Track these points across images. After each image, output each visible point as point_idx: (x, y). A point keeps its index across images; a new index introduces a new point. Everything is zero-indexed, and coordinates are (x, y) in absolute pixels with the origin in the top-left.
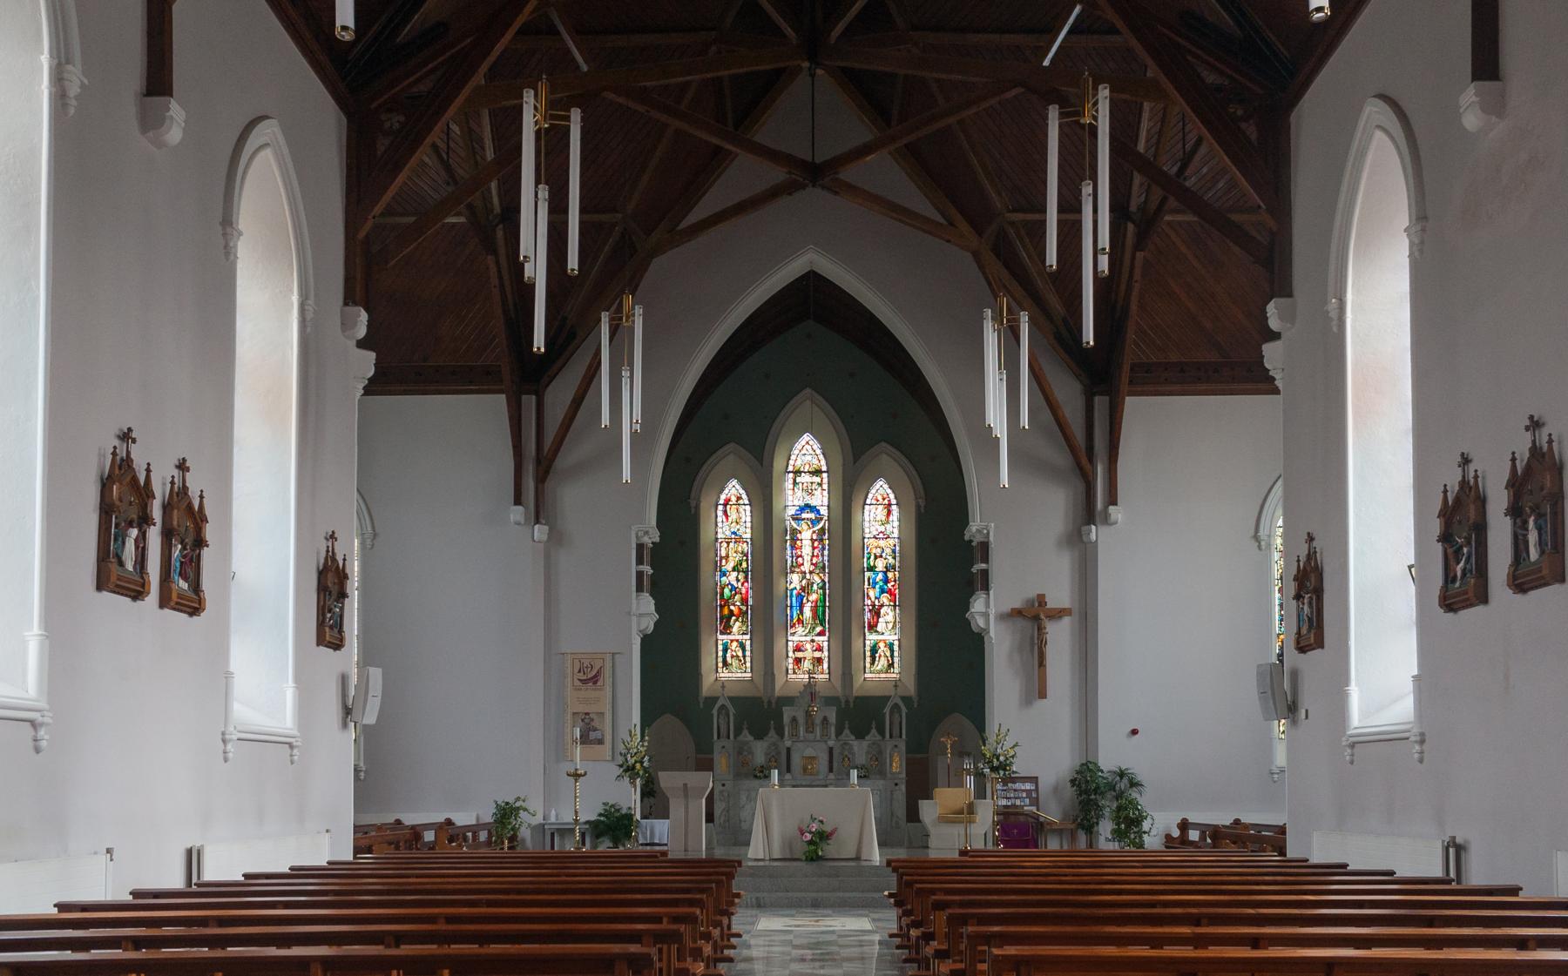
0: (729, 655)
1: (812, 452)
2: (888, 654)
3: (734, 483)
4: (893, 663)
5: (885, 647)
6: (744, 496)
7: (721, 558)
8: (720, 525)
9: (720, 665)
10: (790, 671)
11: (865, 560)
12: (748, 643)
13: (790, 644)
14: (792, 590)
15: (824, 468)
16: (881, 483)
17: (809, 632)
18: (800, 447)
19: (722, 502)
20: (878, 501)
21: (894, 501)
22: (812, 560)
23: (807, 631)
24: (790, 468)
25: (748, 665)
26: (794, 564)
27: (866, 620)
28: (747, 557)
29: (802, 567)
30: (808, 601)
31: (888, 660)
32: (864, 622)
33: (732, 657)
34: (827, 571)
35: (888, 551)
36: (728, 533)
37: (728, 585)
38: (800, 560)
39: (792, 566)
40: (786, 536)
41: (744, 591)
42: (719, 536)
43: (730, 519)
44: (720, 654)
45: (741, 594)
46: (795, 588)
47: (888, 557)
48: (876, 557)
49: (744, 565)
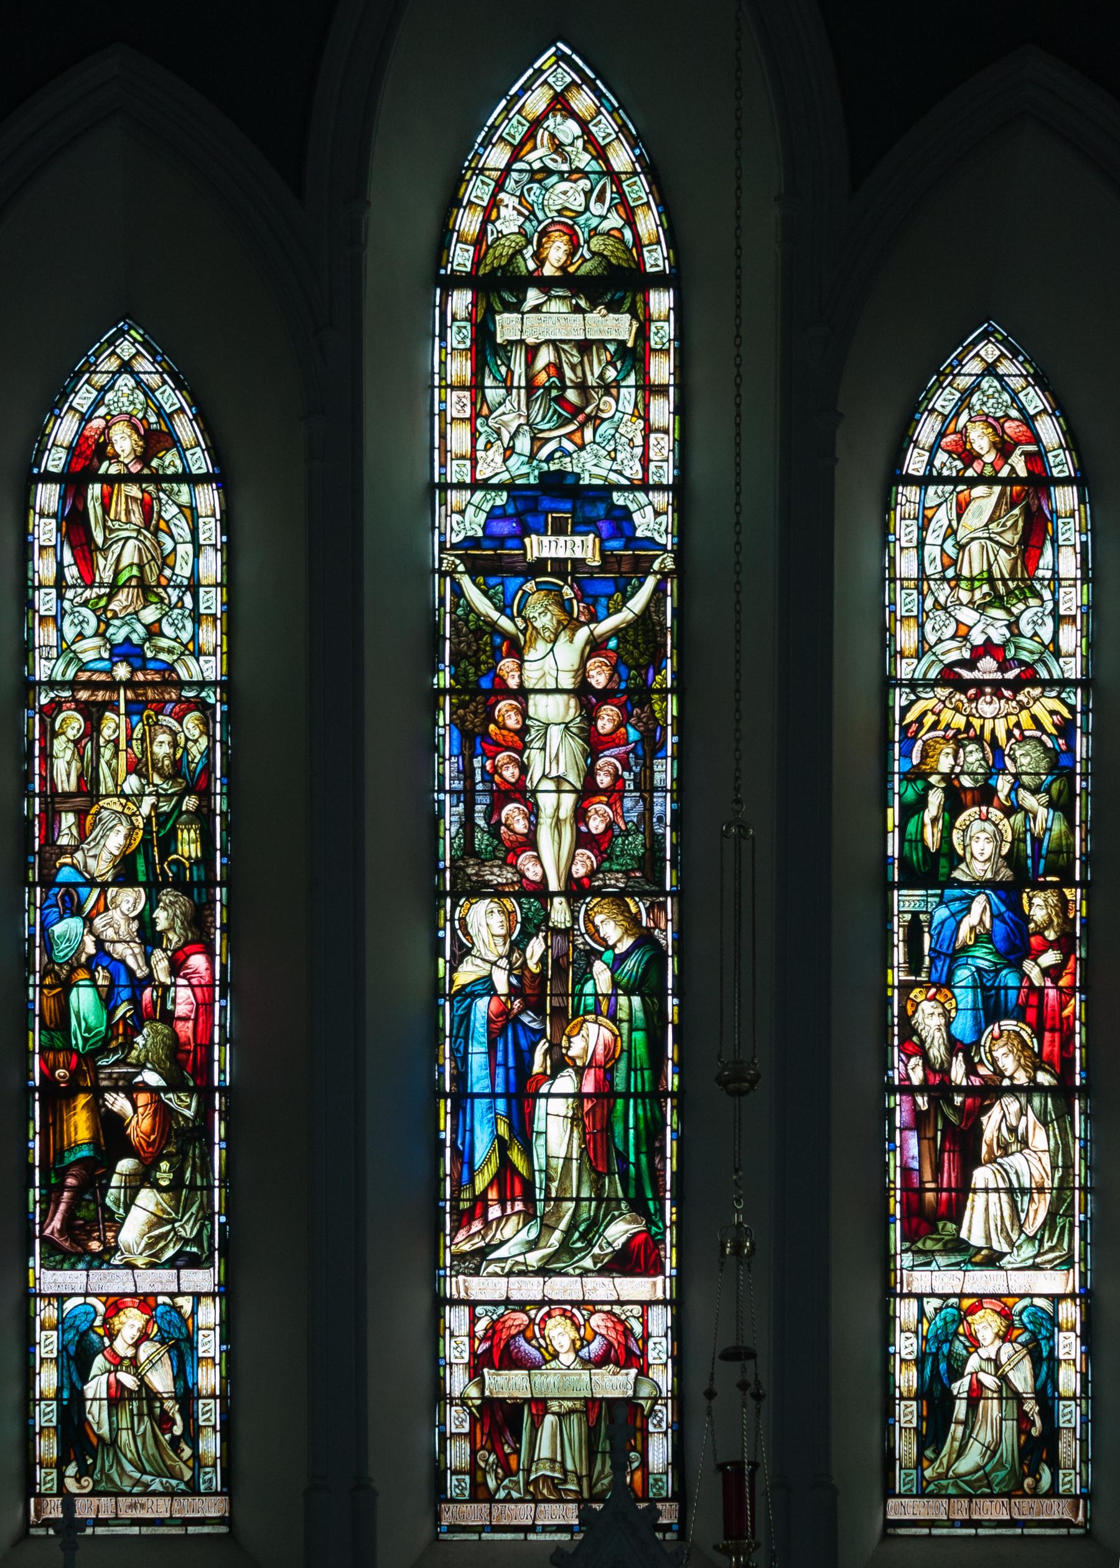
0: (96, 1387)
1: (583, 160)
2: (1022, 1378)
3: (126, 349)
4: (1052, 1432)
5: (1005, 1337)
6: (186, 430)
7: (54, 801)
8: (45, 602)
9: (47, 1447)
10: (455, 1485)
11: (893, 816)
12: (209, 1314)
13: (456, 1319)
14: (468, 994)
15: (656, 259)
16: (990, 352)
17: (565, 1249)
18: (516, 130)
19: (55, 461)
20: (969, 457)
21: (1061, 463)
22: (580, 815)
23: (556, 1237)
24: (461, 258)
25: (210, 1445)
26: (481, 840)
27: (896, 1177)
28: (206, 795)
29: (525, 862)
30: (560, 1064)
31: (1023, 1419)
32: (885, 1193)
33: (117, 1398)
34: (669, 881)
35: (1027, 759)
36: (90, 650)
37: (90, 965)
38: (513, 814)
39: (468, 850)
40: (436, 671)
41: (183, 1000)
42: (42, 670)
43: (104, 570)
44: (47, 1379)
45: (168, 1018)
46: (486, 985)
47: (1029, 800)
48: (955, 802)
49: (188, 845)
